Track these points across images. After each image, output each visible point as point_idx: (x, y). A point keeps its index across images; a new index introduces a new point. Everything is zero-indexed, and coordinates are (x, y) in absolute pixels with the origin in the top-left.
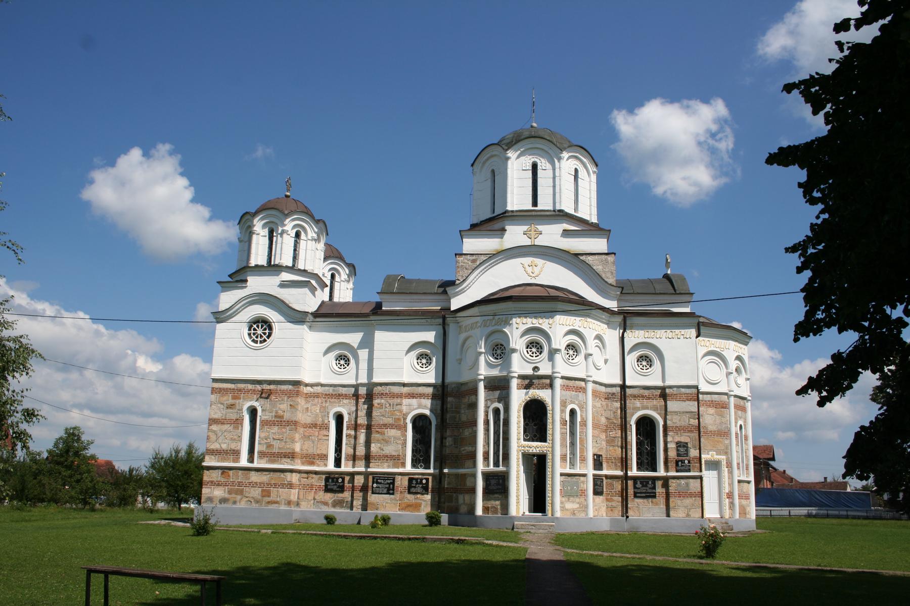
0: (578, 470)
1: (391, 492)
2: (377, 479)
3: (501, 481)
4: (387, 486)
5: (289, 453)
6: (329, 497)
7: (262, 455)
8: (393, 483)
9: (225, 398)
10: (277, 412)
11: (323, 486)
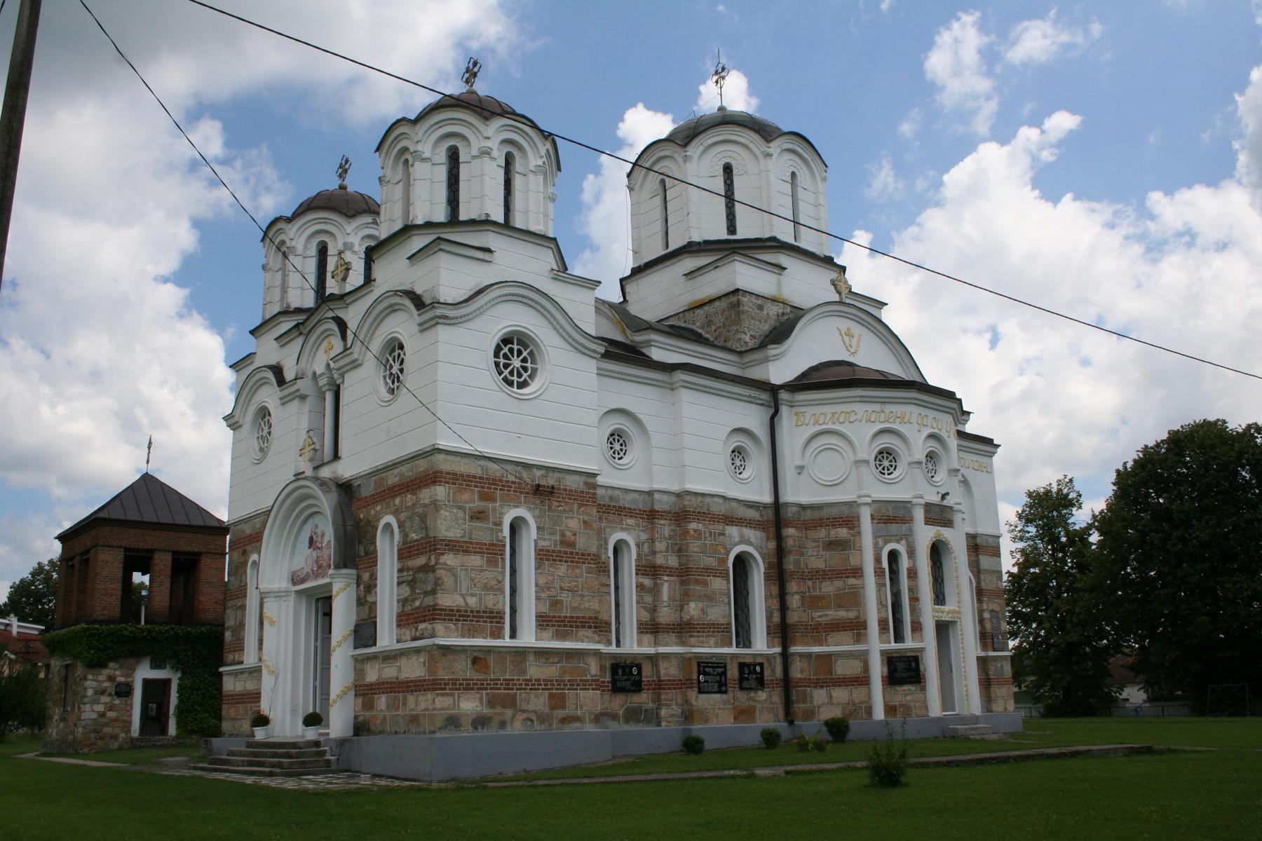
0: (507, 638)
1: (724, 688)
2: (704, 667)
3: (913, 664)
4: (718, 678)
5: (590, 618)
6: (618, 703)
7: (543, 621)
8: (724, 673)
9: (466, 496)
10: (563, 535)
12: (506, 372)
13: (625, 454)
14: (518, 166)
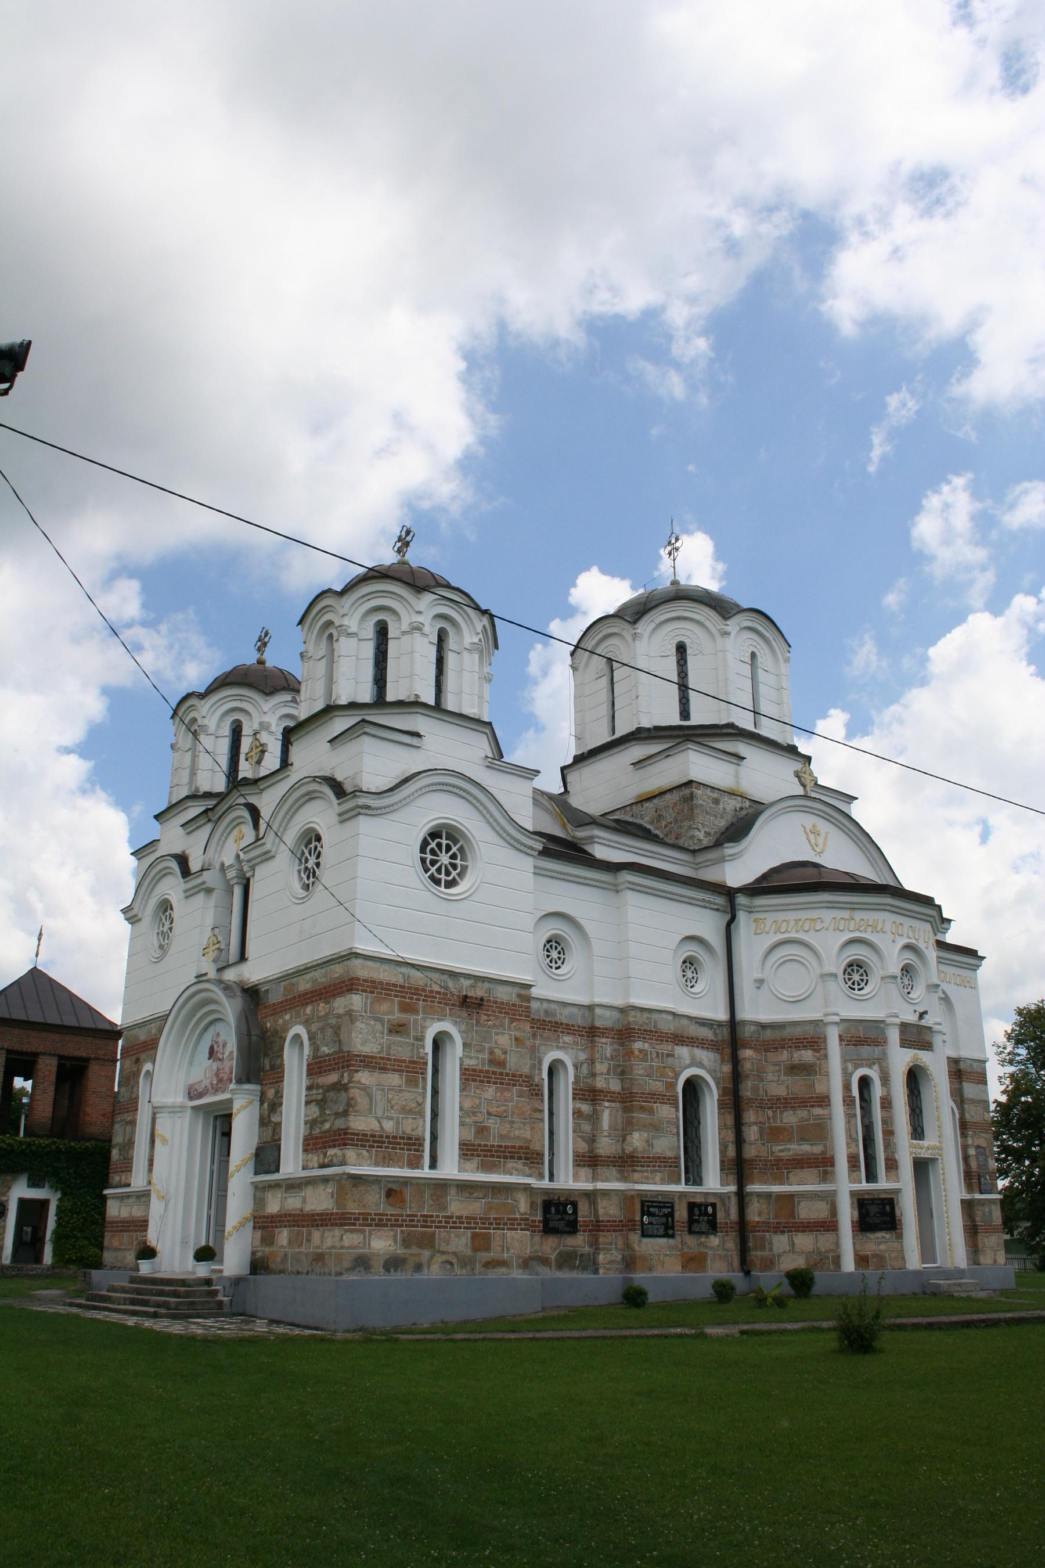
1: (670, 1232)
2: (649, 1207)
3: (888, 1208)
4: (664, 1220)
5: (521, 1147)
6: (550, 1246)
7: (468, 1150)
9: (385, 1007)
10: (491, 1053)
11: (539, 1221)
12: (433, 869)
13: (563, 963)
14: (452, 643)
